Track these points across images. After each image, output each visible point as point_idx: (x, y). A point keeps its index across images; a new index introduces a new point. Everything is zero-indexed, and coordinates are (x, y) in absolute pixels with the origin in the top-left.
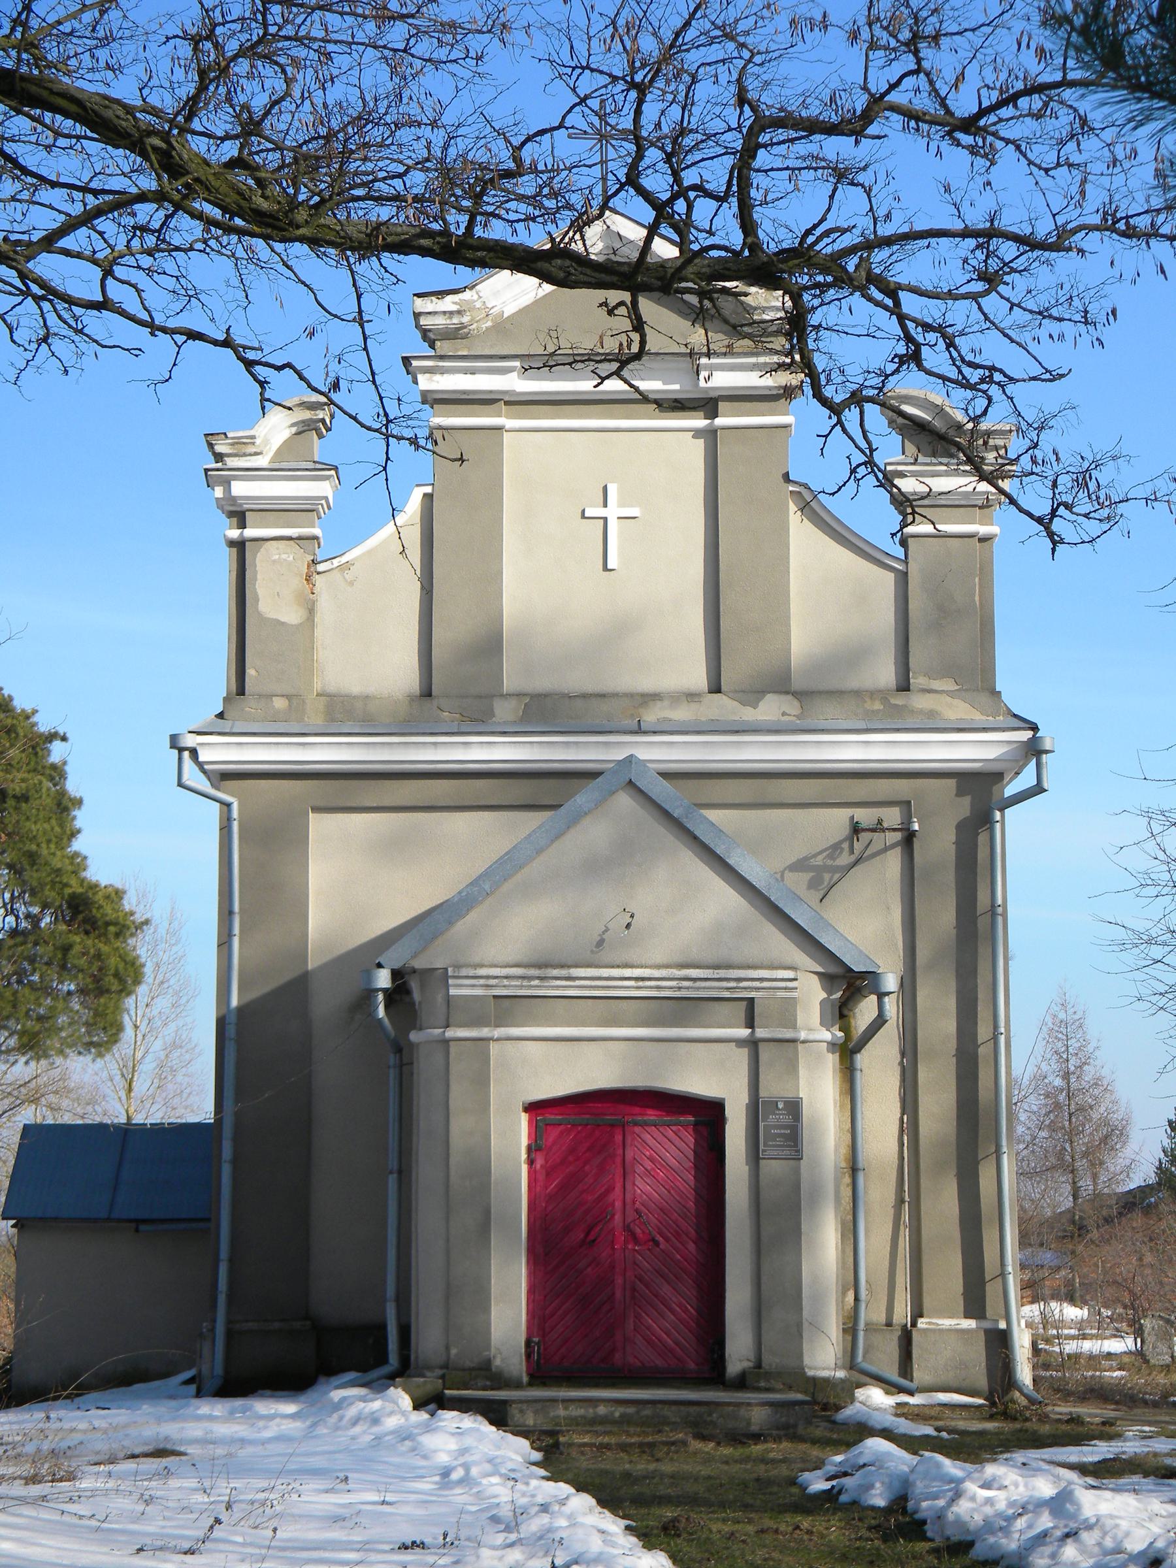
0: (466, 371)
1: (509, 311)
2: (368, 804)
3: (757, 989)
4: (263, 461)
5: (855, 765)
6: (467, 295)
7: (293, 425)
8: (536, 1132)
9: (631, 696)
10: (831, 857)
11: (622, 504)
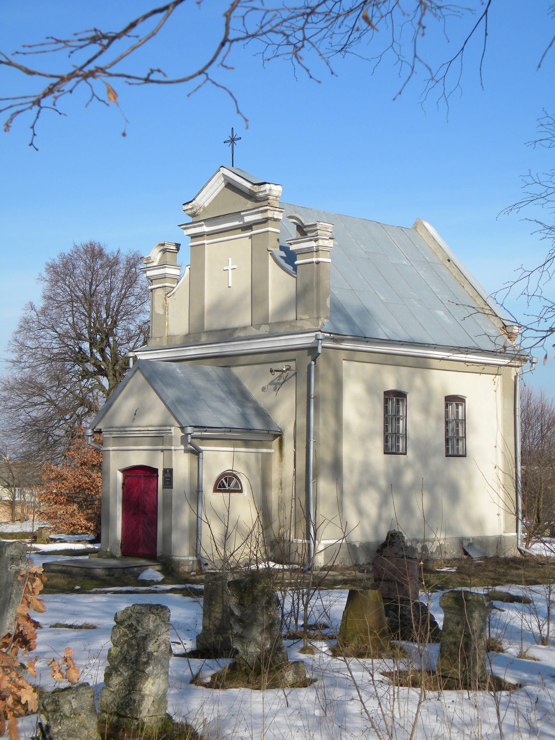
0: (195, 227)
1: (206, 205)
2: (265, 355)
3: (164, 433)
4: (155, 264)
5: (279, 348)
6: (194, 202)
7: (160, 251)
8: (125, 478)
9: (234, 329)
10: (279, 380)
11: (233, 265)
